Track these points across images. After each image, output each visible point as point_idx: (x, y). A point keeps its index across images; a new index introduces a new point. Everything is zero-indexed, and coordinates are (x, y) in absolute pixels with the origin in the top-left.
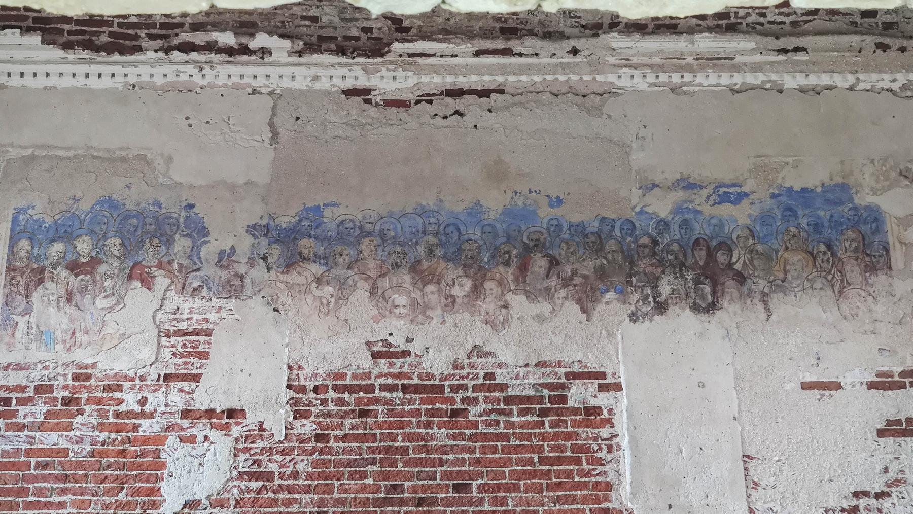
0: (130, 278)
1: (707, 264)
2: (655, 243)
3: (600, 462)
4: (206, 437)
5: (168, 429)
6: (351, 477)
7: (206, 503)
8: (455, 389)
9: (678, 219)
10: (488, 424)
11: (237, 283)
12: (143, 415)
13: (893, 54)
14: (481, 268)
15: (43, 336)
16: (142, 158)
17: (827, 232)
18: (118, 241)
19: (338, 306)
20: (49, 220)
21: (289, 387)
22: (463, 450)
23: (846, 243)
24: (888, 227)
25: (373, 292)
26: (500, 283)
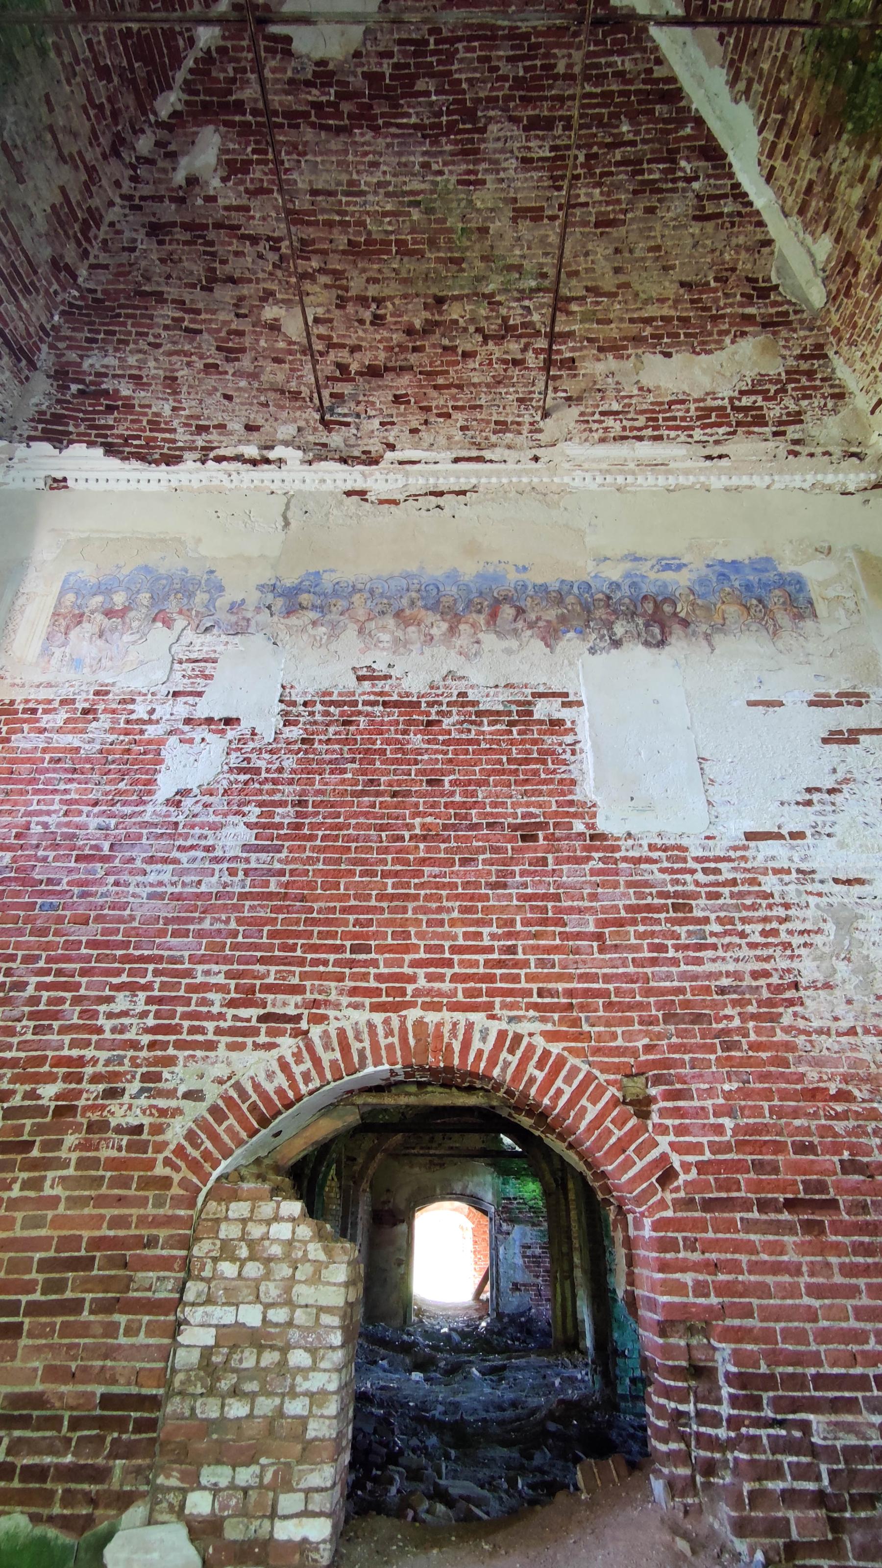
0: (154, 620)
1: (655, 612)
2: (609, 598)
3: (564, 762)
4: (203, 740)
5: (170, 733)
6: (332, 772)
7: (196, 791)
8: (430, 704)
9: (628, 581)
10: (461, 732)
11: (245, 623)
12: (150, 722)
13: (803, 459)
14: (456, 615)
15: (77, 663)
16: (179, 540)
17: (758, 591)
18: (148, 595)
19: (329, 642)
20: (94, 581)
21: (281, 701)
22: (436, 752)
23: (775, 598)
24: (810, 587)
25: (361, 631)
26: (473, 626)
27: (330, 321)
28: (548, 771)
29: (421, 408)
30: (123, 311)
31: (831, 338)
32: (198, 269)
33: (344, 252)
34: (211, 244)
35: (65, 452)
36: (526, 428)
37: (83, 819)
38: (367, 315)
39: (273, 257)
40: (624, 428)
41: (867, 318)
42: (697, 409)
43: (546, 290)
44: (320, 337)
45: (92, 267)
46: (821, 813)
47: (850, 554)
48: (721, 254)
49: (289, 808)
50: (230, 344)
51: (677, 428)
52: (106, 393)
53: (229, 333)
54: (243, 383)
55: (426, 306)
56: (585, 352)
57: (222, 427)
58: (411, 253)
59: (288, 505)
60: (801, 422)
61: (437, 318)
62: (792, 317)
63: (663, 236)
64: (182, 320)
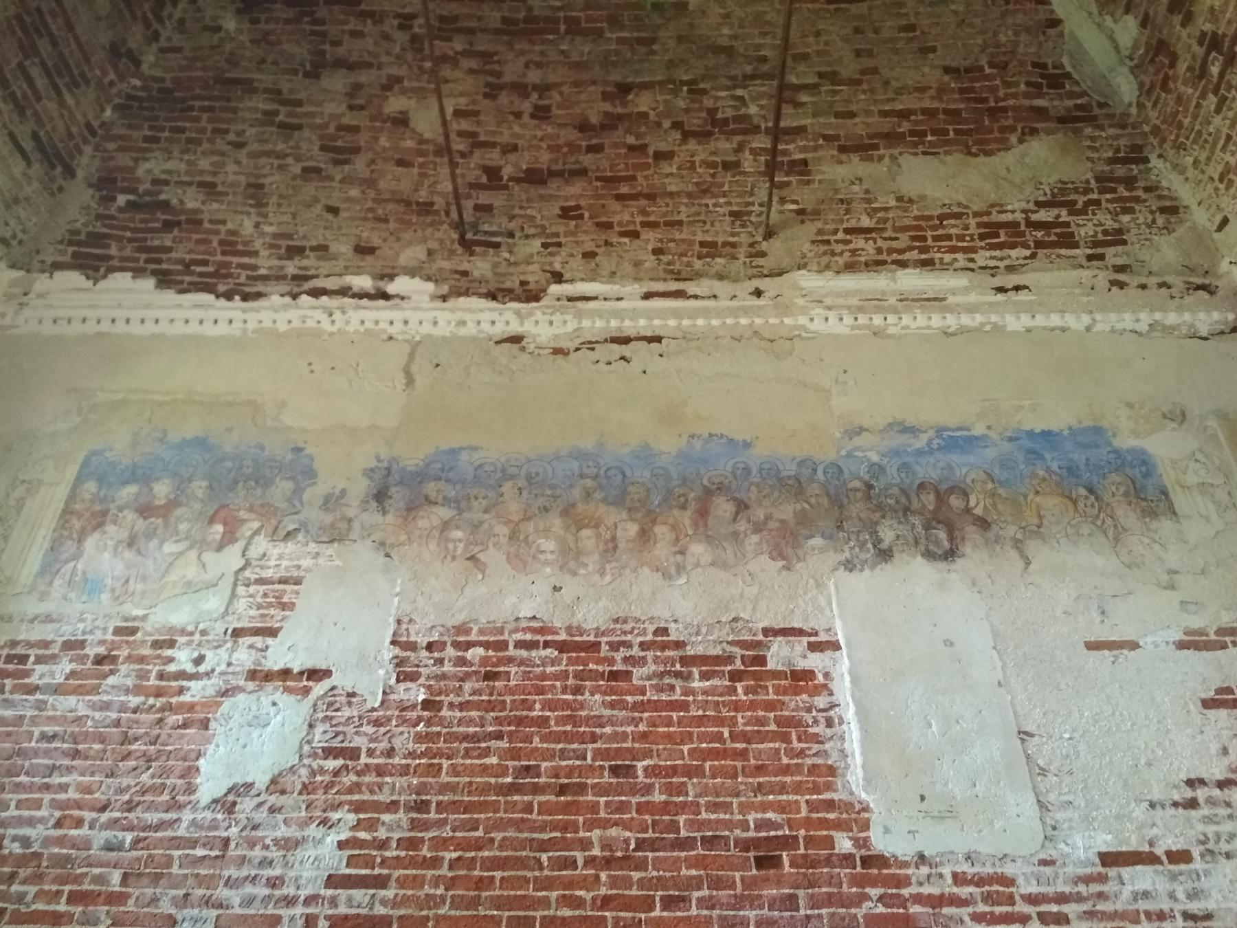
1: (938, 509)
2: (870, 487)
3: (816, 739)
8: (614, 646)
9: (896, 463)
10: (660, 689)
11: (343, 525)
13: (1132, 292)
14: (650, 512)
18: (205, 484)
20: (126, 461)
21: (393, 643)
23: (1113, 484)
24: (1161, 470)
26: (674, 527)
27: (477, 113)
28: (791, 753)
29: (598, 224)
30: (197, 104)
31: (1151, 139)
32: (301, 51)
33: (497, 32)
34: (322, 22)
35: (102, 284)
36: (742, 253)
37: (84, 831)
38: (526, 107)
39: (401, 37)
40: (879, 251)
41: (1195, 117)
42: (979, 225)
43: (768, 77)
44: (461, 134)
45: (163, 50)
46: (1208, 820)
47: (1212, 423)
48: (995, 34)
49: (401, 814)
50: (339, 143)
51: (953, 250)
52: (165, 205)
53: (340, 128)
54: (354, 192)
55: (606, 96)
56: (821, 153)
57: (322, 249)
58: (584, 33)
59: (411, 356)
60: (1124, 243)
61: (620, 110)
62: (1096, 111)
63: (917, 14)
64: (277, 113)
